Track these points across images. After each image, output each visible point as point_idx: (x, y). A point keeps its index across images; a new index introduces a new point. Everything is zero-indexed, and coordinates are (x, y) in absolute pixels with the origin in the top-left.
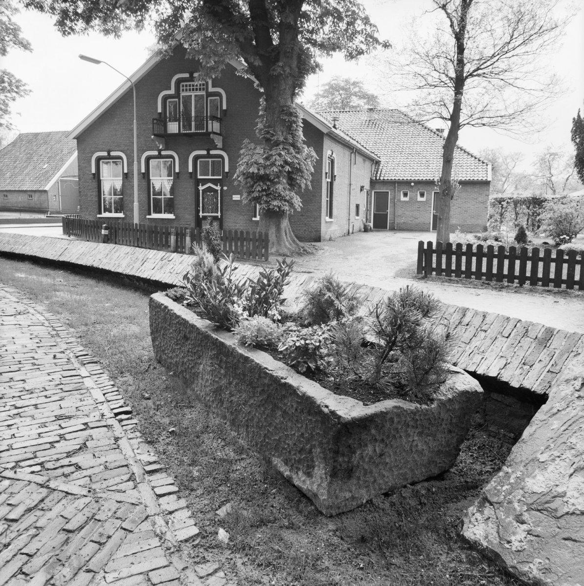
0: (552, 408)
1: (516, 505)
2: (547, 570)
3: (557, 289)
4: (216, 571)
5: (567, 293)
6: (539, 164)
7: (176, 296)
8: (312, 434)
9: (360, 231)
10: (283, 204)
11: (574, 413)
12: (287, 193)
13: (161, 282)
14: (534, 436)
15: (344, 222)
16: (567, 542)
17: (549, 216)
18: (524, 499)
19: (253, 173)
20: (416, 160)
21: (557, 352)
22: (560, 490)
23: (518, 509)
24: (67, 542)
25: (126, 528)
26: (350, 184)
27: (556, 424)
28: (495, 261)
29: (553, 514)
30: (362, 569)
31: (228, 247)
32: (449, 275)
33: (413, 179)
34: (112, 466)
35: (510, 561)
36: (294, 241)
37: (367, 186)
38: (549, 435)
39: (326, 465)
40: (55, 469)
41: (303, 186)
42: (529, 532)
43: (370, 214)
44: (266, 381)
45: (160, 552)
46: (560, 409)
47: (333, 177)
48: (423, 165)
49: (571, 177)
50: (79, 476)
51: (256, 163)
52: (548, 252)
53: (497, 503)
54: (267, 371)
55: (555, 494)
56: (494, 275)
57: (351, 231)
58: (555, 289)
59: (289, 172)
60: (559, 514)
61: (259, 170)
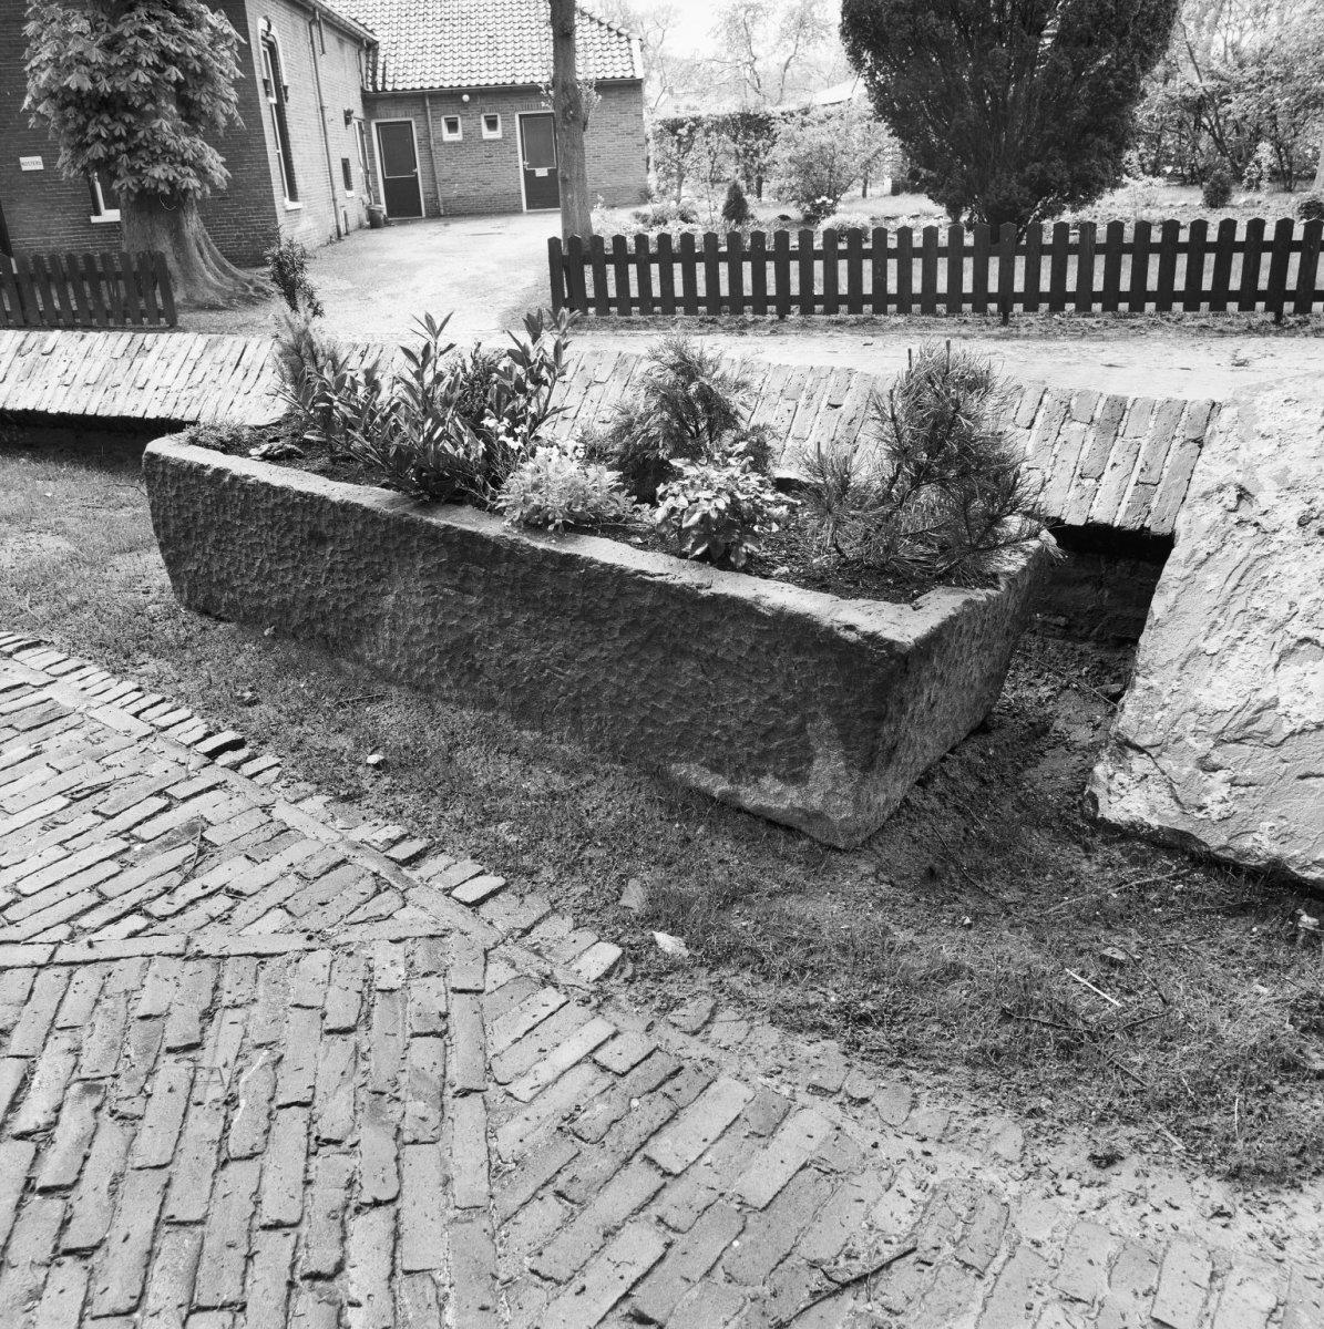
0: (1194, 552)
1: (1191, 740)
2: (1283, 837)
3: (853, 316)
4: (713, 1012)
5: (875, 324)
6: (724, 33)
7: (221, 441)
8: (806, 691)
9: (361, 226)
10: (180, 173)
11: (1239, 554)
12: (186, 141)
13: (45, 414)
14: (1179, 610)
15: (325, 208)
16: (1307, 781)
17: (787, 154)
18: (1204, 728)
19: (79, 90)
20: (464, 35)
21: (1144, 442)
22: (1266, 695)
23: (1198, 746)
24: (359, 1055)
25: (466, 987)
26: (322, 108)
27: (1212, 579)
28: (723, 268)
29: (1266, 741)
30: (970, 926)
31: (40, 301)
32: (625, 311)
33: (464, 84)
34: (313, 869)
35: (1215, 839)
36: (224, 269)
37: (358, 113)
38: (1209, 602)
39: (847, 749)
40: (181, 911)
41: (222, 120)
42: (1233, 782)
43: (376, 182)
44: (647, 601)
45: (576, 1012)
46: (1211, 550)
47: (281, 92)
48: (482, 47)
49: (792, 60)
50: (254, 913)
51: (81, 60)
52: (782, 238)
53: (1152, 746)
54: (646, 578)
55: (1259, 705)
56: (723, 300)
57: (343, 230)
58: (849, 317)
59: (178, 84)
60: (1276, 738)
61: (93, 80)
